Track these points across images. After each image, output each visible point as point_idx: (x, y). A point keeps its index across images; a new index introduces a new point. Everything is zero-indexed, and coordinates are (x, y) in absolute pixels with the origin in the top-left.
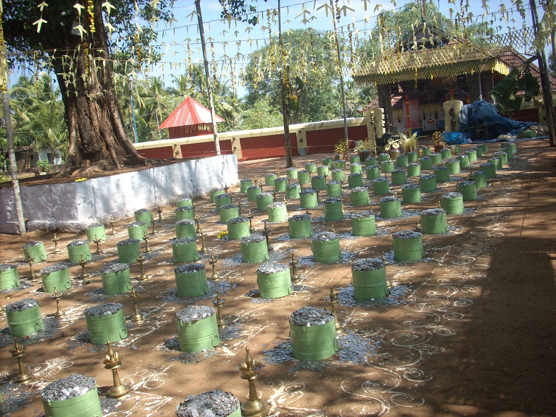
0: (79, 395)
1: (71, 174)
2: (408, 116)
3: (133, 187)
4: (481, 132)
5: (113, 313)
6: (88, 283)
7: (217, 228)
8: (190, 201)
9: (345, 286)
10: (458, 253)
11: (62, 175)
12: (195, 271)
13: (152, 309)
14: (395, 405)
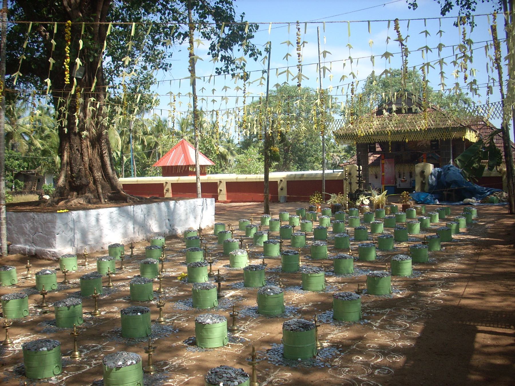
1: (57, 204)
2: (384, 174)
3: (111, 222)
4: (448, 194)
5: (48, 350)
6: (46, 312)
7: (180, 269)
8: (163, 239)
10: (394, 317)
11: (49, 204)
12: (139, 314)
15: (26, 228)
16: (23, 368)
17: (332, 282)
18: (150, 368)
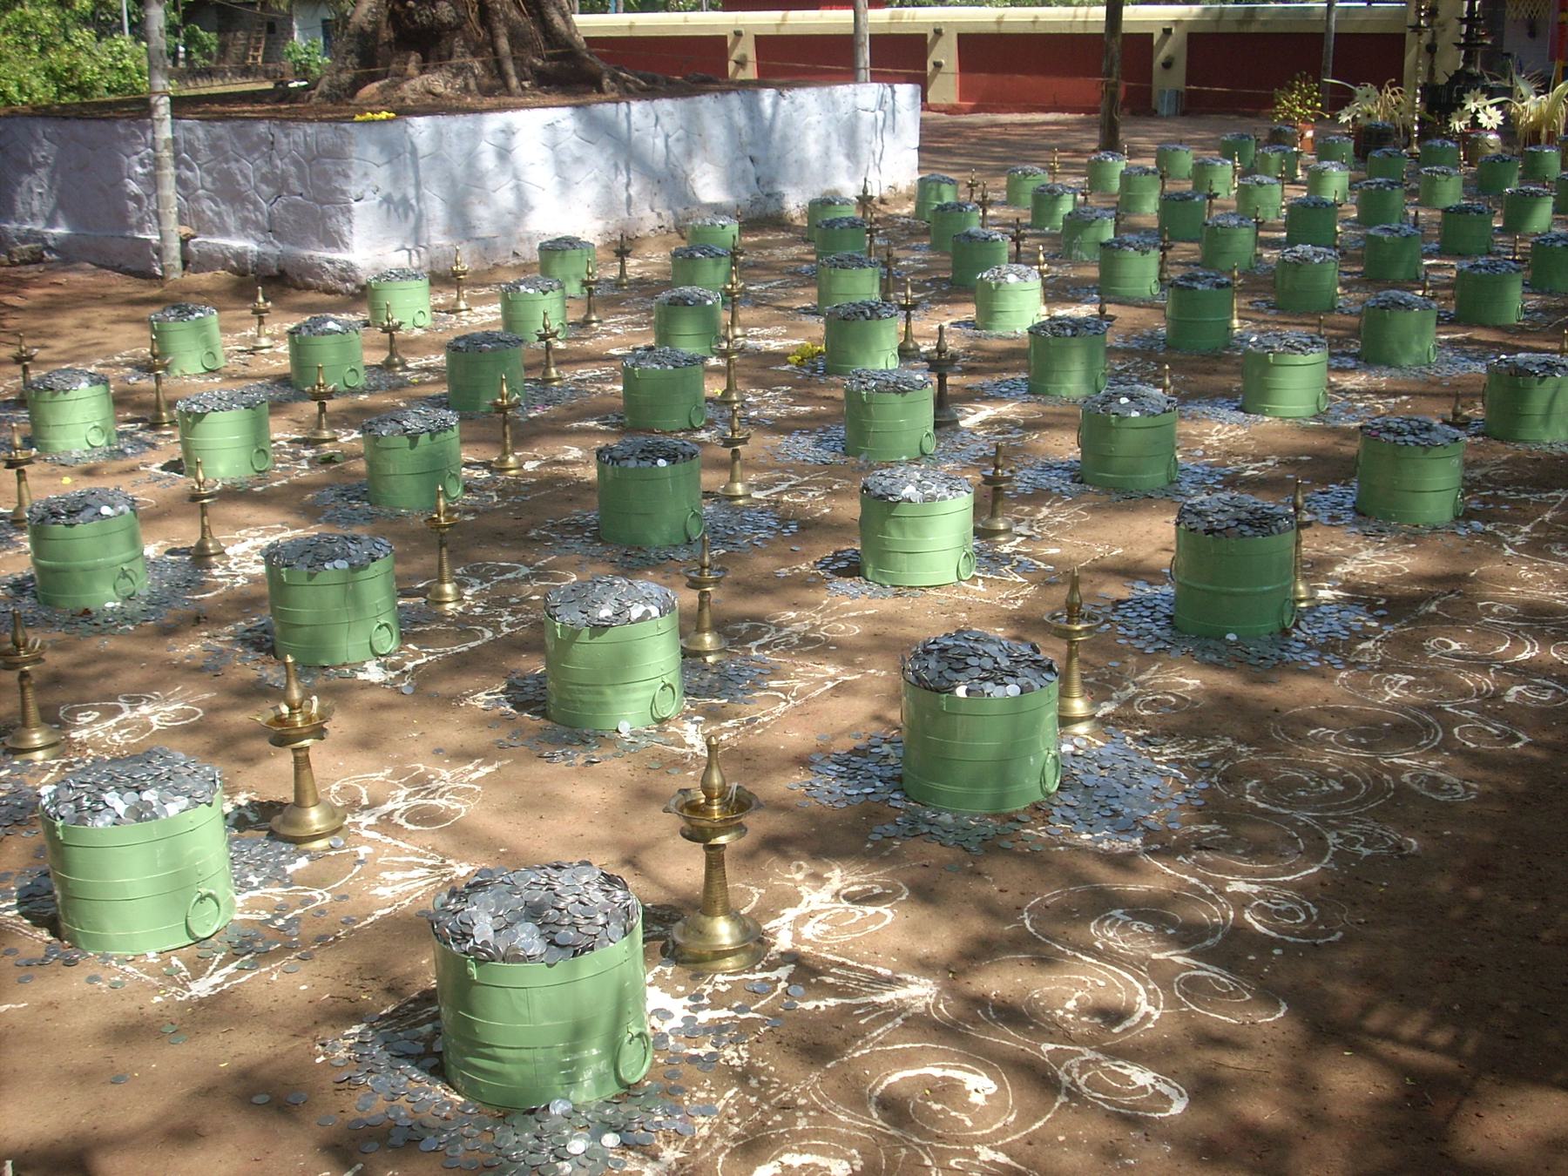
0: (155, 816)
1: (353, 96)
8: (733, 227)
12: (662, 463)
13: (504, 570)
14: (1182, 1004)
15: (245, 177)
16: (265, 632)
17: (1353, 391)
18: (702, 641)
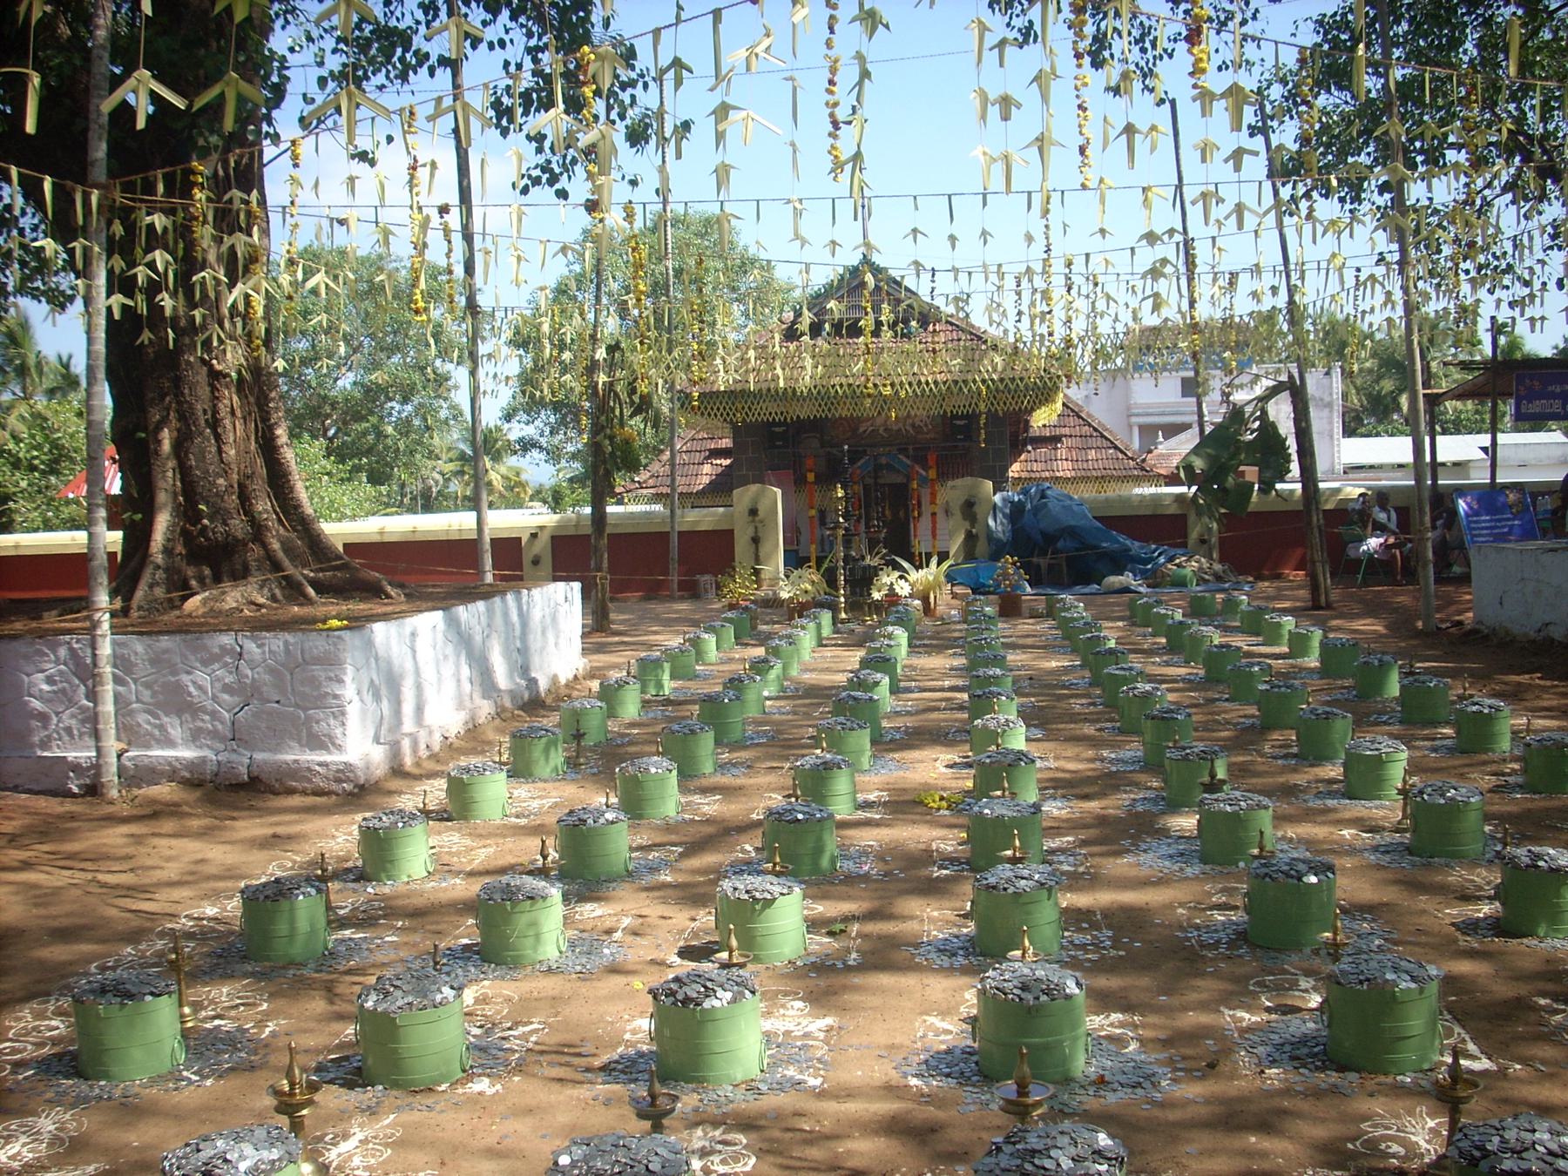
9: (535, 949)
